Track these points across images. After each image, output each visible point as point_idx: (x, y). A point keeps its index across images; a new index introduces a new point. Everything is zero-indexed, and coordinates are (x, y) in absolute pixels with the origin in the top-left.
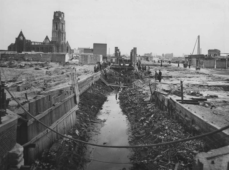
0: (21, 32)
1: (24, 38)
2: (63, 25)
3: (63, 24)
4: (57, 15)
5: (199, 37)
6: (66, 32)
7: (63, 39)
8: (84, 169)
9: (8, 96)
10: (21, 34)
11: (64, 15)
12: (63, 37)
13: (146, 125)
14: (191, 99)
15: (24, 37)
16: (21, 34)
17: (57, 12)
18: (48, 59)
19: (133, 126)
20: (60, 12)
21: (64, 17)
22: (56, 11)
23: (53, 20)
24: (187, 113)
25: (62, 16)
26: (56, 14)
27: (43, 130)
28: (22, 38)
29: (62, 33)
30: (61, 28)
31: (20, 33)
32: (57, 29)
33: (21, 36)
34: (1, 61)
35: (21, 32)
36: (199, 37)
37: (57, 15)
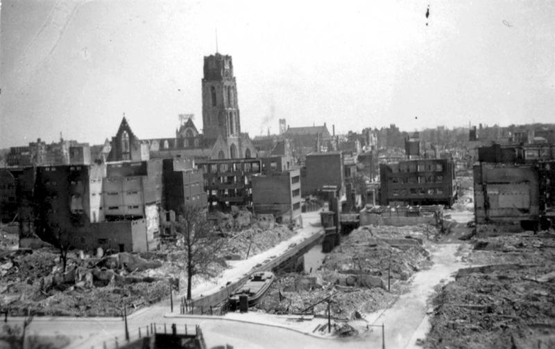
0: (124, 122)
1: (131, 136)
2: (232, 91)
3: (229, 88)
4: (213, 66)
5: (333, 126)
7: (234, 129)
8: (6, 312)
10: (124, 126)
11: (230, 63)
12: (234, 124)
13: (124, 275)
16: (124, 126)
18: (313, 199)
22: (208, 55)
23: (203, 80)
25: (227, 67)
28: (127, 135)
29: (231, 114)
30: (225, 99)
32: (214, 104)
33: (125, 132)
34: (551, 281)
35: (124, 122)
36: (333, 126)
37: (213, 66)
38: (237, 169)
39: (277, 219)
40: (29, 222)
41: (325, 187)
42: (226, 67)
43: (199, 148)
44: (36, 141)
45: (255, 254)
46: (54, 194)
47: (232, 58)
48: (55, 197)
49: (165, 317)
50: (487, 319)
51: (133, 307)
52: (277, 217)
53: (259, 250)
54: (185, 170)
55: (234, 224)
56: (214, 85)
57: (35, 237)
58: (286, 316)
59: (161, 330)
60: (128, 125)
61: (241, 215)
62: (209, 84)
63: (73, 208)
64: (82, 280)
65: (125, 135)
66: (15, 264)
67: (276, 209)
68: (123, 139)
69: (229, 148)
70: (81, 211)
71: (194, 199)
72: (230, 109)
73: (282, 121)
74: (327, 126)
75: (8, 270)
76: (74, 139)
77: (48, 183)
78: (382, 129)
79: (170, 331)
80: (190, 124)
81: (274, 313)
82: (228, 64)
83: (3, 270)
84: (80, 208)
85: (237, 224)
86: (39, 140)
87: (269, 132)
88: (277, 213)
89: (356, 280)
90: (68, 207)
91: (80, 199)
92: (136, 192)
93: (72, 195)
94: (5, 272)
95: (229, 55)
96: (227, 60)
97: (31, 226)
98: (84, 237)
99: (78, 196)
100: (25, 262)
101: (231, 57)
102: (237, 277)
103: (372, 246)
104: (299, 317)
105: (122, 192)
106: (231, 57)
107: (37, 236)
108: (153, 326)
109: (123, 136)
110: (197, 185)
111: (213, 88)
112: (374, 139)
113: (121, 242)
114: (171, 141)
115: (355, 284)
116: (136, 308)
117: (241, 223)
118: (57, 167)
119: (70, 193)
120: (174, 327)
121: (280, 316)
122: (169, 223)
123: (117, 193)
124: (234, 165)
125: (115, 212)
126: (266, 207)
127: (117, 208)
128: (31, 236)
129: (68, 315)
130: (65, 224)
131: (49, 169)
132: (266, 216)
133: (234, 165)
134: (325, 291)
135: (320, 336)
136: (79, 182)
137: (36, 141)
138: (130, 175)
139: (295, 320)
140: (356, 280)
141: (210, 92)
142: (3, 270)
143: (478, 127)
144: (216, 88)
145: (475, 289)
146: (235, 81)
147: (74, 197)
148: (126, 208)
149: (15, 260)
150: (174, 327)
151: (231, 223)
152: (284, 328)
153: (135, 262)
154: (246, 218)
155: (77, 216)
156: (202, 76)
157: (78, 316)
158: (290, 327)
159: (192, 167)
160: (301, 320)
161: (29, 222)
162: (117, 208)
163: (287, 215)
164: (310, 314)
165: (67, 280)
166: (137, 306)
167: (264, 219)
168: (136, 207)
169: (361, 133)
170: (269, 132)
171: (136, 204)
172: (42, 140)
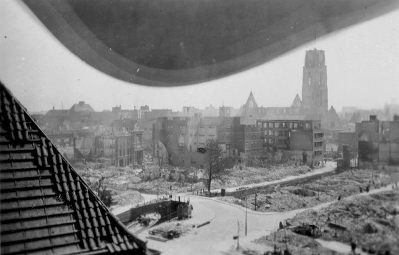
1: (255, 104)
11: (323, 55)
23: (304, 67)
28: (252, 104)
33: (251, 102)
35: (251, 94)
44: (209, 106)
66: (144, 170)
68: (250, 107)
79: (177, 200)
80: (297, 96)
84: (183, 142)
86: (211, 105)
87: (54, 108)
95: (323, 50)
98: (185, 160)
100: (149, 169)
113: (190, 163)
114: (287, 109)
122: (235, 156)
135: (14, 149)
136: (184, 127)
137: (209, 106)
145: (149, 164)
149: (143, 168)
155: (182, 147)
156: (303, 65)
169: (111, 110)
170: (54, 108)
172: (213, 106)
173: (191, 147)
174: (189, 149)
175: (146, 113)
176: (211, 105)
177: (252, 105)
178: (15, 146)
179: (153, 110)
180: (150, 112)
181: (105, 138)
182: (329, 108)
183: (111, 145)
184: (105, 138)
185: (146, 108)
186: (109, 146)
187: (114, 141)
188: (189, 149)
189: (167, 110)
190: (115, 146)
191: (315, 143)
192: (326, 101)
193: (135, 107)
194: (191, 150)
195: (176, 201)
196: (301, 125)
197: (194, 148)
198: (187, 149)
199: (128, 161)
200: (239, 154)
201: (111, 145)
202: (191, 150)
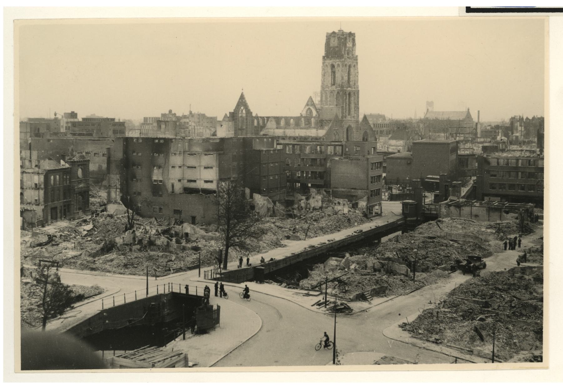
0: (242, 97)
1: (249, 112)
5: (479, 111)
6: (360, 89)
9: (272, 271)
10: (242, 102)
11: (354, 40)
12: (352, 106)
14: (285, 246)
15: (249, 110)
16: (242, 102)
17: (334, 33)
19: (459, 319)
20: (343, 33)
21: (354, 44)
22: (330, 31)
24: (502, 293)
25: (349, 44)
26: (332, 40)
27: (528, 273)
28: (244, 111)
29: (349, 94)
31: (240, 99)
33: (242, 108)
35: (242, 97)
37: (334, 42)
38: (522, 164)
39: (353, 205)
40: (116, 188)
41: (429, 176)
42: (348, 45)
43: (314, 128)
44: (167, 112)
45: (316, 237)
46: (139, 165)
47: (356, 35)
48: (140, 167)
49: (190, 280)
50: (471, 311)
51: (170, 270)
52: (354, 202)
53: (321, 233)
54: (264, 149)
55: (306, 206)
56: (334, 63)
57: (119, 203)
58: (296, 291)
59: (176, 290)
60: (245, 101)
61: (313, 198)
62: (329, 62)
63: (155, 178)
64: (138, 244)
65: (242, 111)
67: (354, 194)
68: (240, 115)
69: (345, 130)
70: (161, 181)
71: (271, 178)
72: (349, 89)
73: (430, 104)
74: (471, 111)
75: (88, 231)
76: (202, 113)
77: (135, 154)
78: (534, 118)
79: (184, 291)
81: (285, 287)
82: (351, 40)
83: (84, 230)
84: (161, 179)
85: (308, 206)
88: (355, 198)
89: (383, 267)
90: (150, 177)
91: (161, 170)
92: (212, 168)
93: (154, 167)
94: (86, 232)
95: (352, 32)
96: (350, 37)
97: (118, 193)
99: (159, 167)
101: (354, 34)
102: (284, 255)
103: (431, 238)
104: (306, 292)
105: (200, 166)
106: (354, 34)
107: (121, 203)
108: (170, 285)
109: (240, 112)
110: (277, 164)
111: (333, 66)
112: (519, 128)
113: (193, 215)
115: (382, 270)
116: (172, 271)
117: (313, 206)
118: (143, 138)
119: (153, 164)
120: (187, 288)
121: (290, 290)
123: (195, 167)
124: (318, 147)
125: (192, 185)
126: (343, 191)
127: (195, 181)
128: (116, 202)
129: (109, 272)
130: (146, 194)
131: (514, 161)
132: (341, 201)
133: (318, 147)
134: (355, 274)
137: (167, 112)
138: (208, 150)
139: (302, 295)
140: (383, 265)
141: (330, 71)
142: (84, 230)
143: (525, 118)
144: (336, 67)
146: (357, 60)
147: (155, 168)
148: (203, 182)
150: (187, 288)
151: (303, 205)
152: (457, 348)
153: (196, 233)
154: (317, 201)
156: (323, 53)
157: (121, 274)
158: (293, 299)
159: (273, 147)
160: (308, 295)
161: (116, 188)
162: (195, 181)
163: (363, 201)
164: (318, 291)
165: (125, 242)
166: (173, 270)
167: (339, 203)
168: (211, 182)
171: (210, 178)
172: (173, 112)
173: (173, 186)
174: (170, 190)
175: (74, 124)
176: (170, 111)
177: (243, 113)
178: (455, 344)
179: (83, 119)
180: (79, 122)
181: (26, 173)
182: (361, 117)
183: (36, 184)
184: (26, 173)
185: (73, 115)
186: (34, 186)
187: (42, 178)
188: (170, 190)
189: (542, 208)
190: (42, 186)
191: (372, 177)
192: (357, 108)
193: (55, 115)
194: (173, 192)
195: (180, 294)
196: (347, 150)
197: (178, 187)
198: (167, 191)
199: (65, 210)
200: (251, 197)
201: (36, 184)
202: (173, 192)
